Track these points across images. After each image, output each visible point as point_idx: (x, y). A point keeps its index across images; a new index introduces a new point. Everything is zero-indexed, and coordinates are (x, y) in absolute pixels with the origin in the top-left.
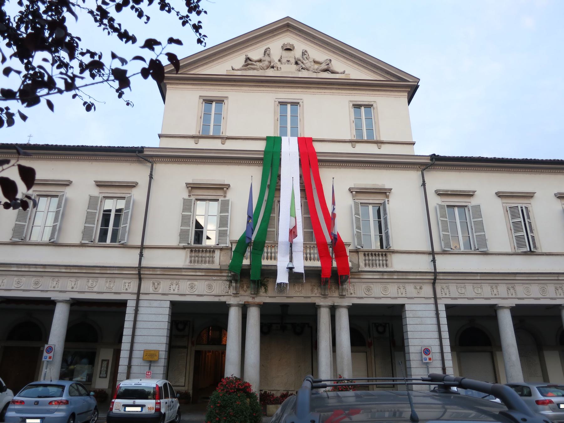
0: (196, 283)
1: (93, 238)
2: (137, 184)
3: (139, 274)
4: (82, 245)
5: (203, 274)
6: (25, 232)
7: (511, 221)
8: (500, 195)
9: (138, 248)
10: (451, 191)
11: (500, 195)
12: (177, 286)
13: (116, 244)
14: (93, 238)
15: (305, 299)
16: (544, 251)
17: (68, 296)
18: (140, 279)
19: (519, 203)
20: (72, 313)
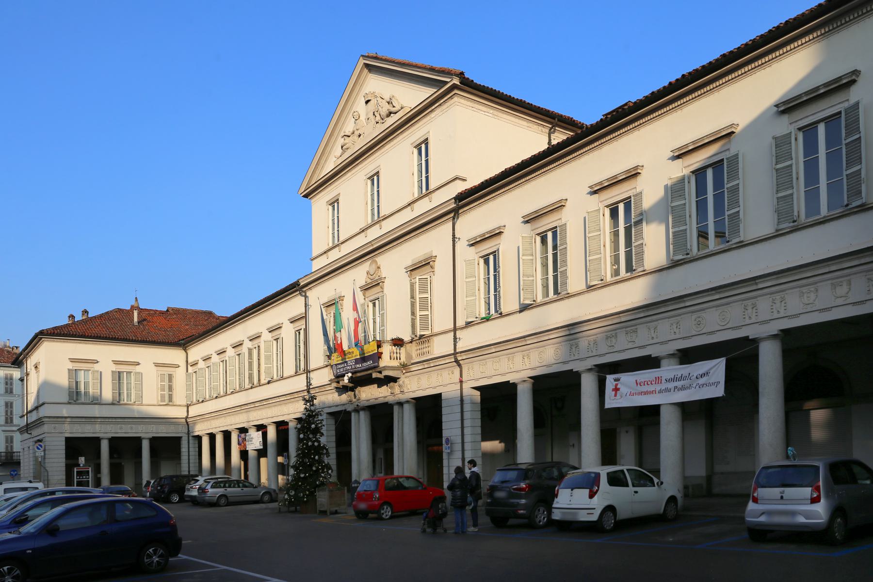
0: (703, 314)
1: (796, 213)
2: (856, 72)
3: (457, 361)
4: (778, 235)
5: (642, 315)
6: (671, 246)
7: (794, 161)
8: (157, 365)
9: (450, 331)
10: (826, 85)
11: (157, 365)
12: (754, 311)
13: (635, 274)
14: (796, 213)
15: (734, 332)
16: (178, 403)
17: (775, 328)
18: (459, 365)
19: (167, 371)
20: (787, 353)
